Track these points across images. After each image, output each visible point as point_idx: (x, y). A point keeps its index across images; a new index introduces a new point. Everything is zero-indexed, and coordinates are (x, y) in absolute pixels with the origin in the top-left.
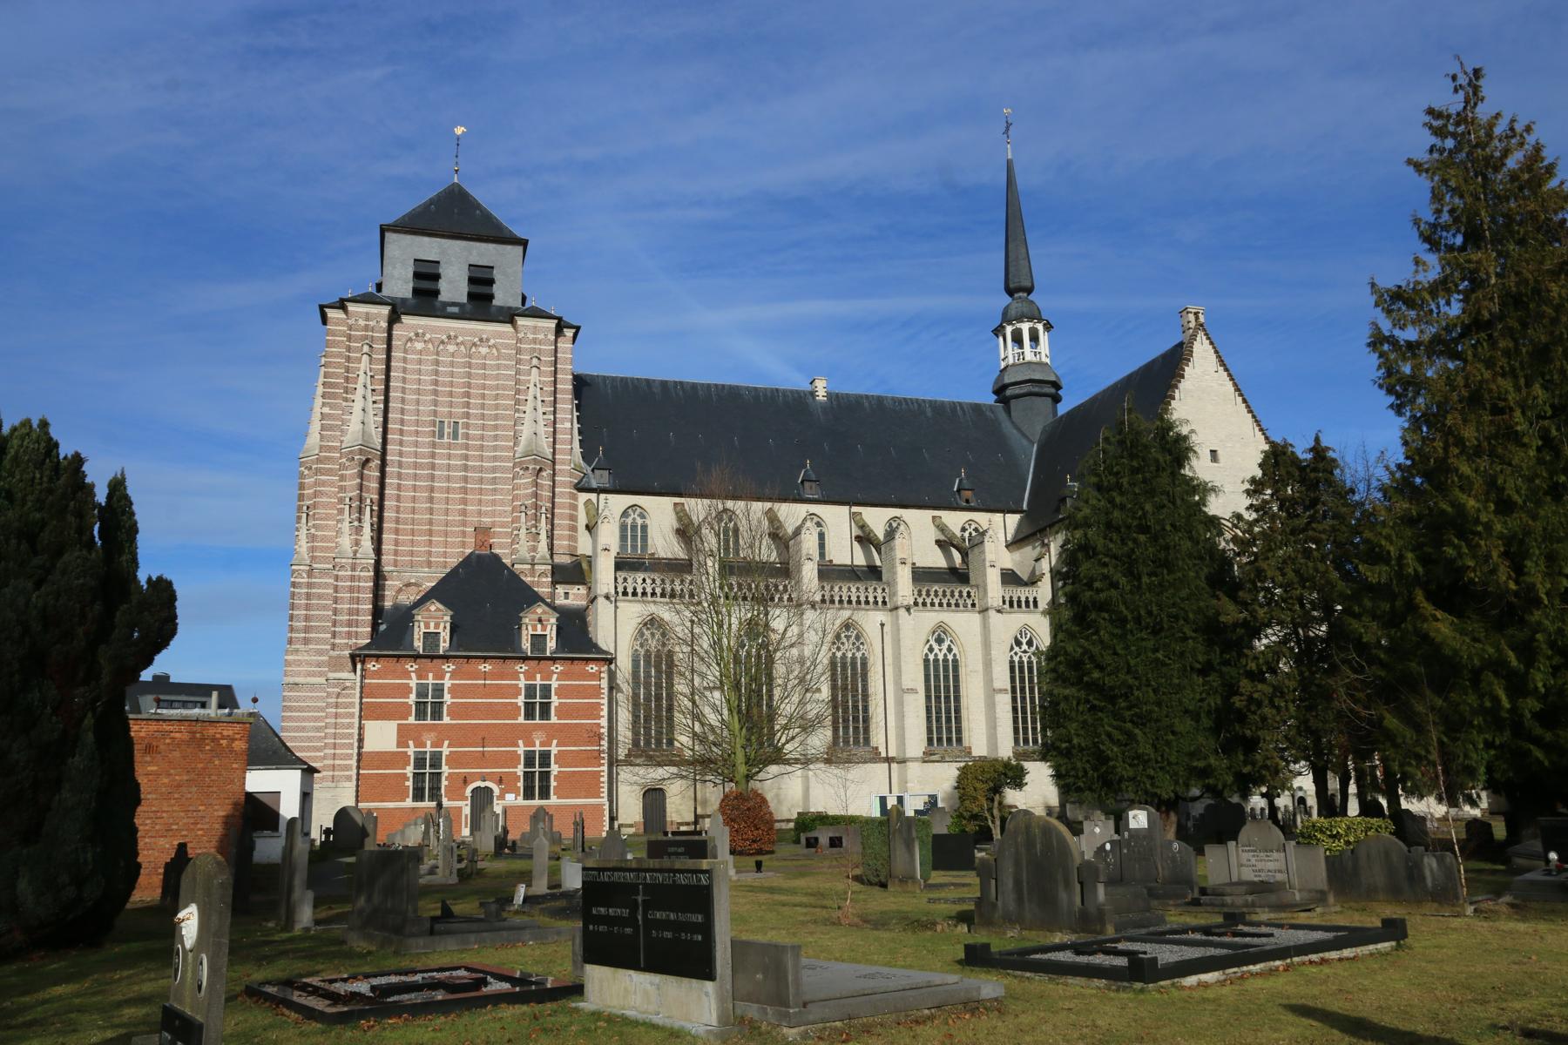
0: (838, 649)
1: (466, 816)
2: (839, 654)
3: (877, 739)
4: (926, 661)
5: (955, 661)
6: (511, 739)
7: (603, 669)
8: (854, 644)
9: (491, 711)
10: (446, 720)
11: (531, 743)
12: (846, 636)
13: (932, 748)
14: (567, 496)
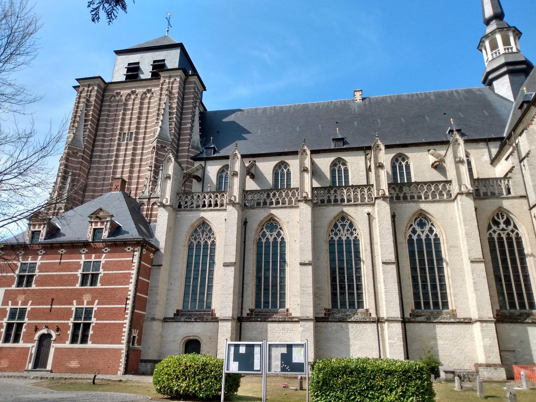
0: (336, 234)
1: (31, 354)
2: (336, 239)
3: (368, 302)
4: (491, 240)
5: (437, 239)
6: (68, 299)
7: (136, 249)
8: (348, 230)
9: (61, 280)
10: (99, 286)
11: (80, 302)
12: (341, 225)
13: (419, 311)
14: (185, 163)
